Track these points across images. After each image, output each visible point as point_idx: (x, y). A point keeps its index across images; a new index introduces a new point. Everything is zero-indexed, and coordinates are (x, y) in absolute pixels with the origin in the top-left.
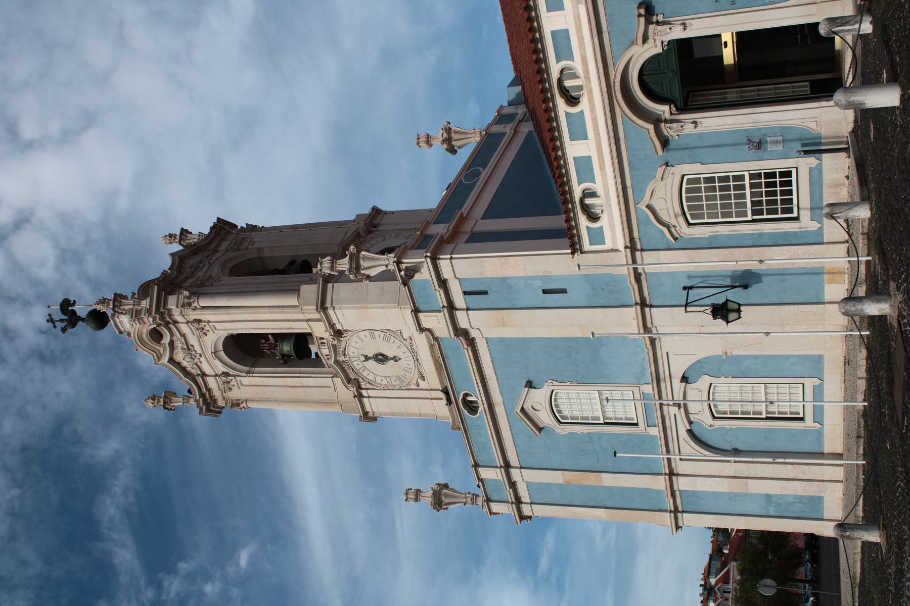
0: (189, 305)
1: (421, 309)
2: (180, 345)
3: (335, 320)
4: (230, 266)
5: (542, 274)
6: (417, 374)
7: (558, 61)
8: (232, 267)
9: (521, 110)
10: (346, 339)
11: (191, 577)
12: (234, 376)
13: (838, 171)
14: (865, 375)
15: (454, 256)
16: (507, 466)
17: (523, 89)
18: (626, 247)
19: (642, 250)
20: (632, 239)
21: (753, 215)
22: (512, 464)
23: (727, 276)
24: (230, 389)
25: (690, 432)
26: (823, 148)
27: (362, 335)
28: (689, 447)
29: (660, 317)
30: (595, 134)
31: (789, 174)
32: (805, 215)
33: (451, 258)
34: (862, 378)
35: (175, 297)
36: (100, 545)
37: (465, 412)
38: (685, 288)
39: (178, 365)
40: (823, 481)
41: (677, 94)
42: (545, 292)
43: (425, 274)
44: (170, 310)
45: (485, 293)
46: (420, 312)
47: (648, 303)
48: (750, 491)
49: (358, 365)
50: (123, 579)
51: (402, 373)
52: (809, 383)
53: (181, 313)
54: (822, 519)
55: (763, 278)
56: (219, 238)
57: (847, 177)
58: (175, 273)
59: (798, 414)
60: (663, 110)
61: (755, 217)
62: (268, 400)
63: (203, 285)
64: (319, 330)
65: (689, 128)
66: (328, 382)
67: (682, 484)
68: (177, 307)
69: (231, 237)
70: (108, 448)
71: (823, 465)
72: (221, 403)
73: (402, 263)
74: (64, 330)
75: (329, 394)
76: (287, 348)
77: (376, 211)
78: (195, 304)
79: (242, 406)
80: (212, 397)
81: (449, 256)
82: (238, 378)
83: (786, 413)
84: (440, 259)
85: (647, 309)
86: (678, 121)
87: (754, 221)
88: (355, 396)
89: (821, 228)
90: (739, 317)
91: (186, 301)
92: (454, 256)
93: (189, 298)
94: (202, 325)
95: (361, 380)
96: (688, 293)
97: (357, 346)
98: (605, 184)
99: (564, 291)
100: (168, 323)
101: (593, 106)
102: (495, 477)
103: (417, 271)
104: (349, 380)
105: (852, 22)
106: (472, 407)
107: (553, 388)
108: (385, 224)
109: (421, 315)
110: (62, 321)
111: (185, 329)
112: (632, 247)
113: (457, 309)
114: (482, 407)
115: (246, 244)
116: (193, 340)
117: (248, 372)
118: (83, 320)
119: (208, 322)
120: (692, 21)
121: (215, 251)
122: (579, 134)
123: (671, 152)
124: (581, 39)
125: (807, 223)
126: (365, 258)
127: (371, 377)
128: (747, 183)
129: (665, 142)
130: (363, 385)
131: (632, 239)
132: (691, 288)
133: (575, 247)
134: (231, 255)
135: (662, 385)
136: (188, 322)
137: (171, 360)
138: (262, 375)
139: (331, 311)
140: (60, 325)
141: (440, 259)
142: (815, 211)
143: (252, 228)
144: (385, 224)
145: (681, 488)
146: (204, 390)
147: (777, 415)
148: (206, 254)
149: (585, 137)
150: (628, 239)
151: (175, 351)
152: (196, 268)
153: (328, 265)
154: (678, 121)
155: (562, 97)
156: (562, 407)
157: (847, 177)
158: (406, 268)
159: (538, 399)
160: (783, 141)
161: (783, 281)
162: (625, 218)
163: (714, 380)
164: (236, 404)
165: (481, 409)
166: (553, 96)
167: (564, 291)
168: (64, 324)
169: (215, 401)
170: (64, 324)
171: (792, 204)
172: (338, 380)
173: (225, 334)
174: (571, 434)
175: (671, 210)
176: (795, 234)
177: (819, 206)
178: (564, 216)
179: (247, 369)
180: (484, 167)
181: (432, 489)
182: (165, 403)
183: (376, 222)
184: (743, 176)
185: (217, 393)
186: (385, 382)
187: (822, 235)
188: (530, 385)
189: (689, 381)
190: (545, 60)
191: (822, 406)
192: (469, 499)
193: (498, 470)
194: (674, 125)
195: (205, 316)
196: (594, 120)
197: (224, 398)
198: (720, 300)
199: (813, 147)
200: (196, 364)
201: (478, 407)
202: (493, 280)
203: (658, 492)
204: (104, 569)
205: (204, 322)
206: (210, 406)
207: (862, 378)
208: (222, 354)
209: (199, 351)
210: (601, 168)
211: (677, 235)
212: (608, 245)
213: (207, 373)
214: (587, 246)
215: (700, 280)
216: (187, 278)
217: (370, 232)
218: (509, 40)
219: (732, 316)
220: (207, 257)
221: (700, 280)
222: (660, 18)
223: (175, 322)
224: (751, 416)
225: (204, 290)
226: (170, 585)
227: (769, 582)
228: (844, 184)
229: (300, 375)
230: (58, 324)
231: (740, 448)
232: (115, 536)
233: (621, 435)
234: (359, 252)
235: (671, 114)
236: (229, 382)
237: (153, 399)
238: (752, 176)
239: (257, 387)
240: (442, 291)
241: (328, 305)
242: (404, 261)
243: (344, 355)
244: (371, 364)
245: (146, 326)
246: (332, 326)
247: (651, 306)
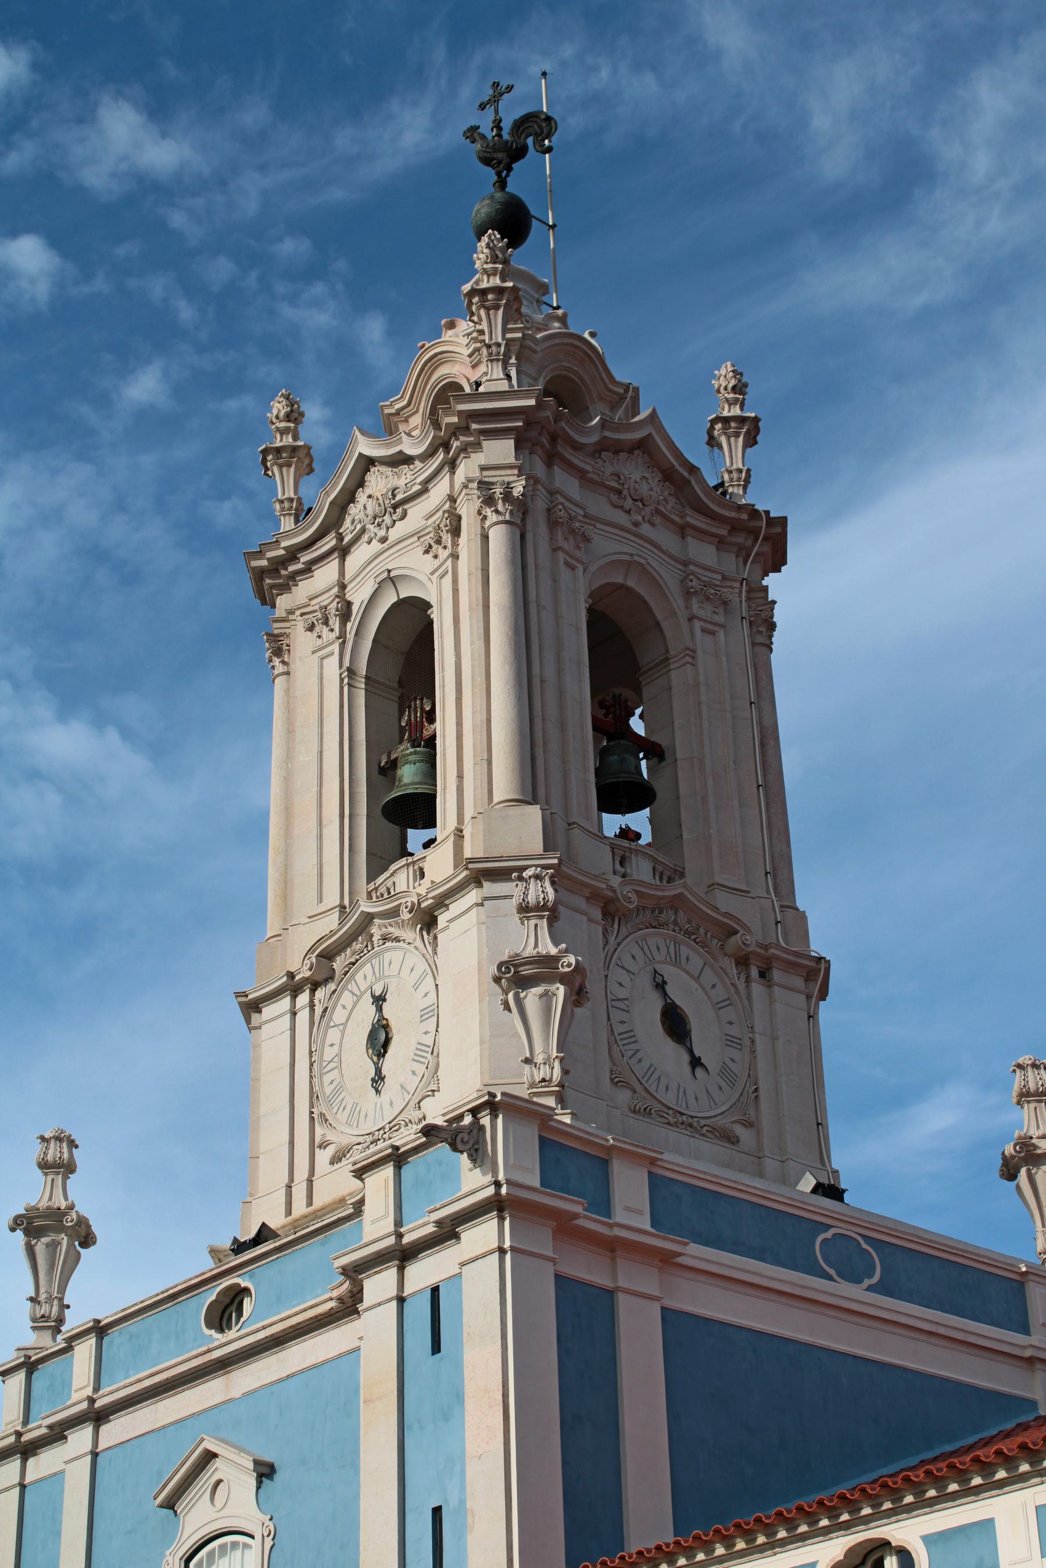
0: (489, 501)
1: (406, 1170)
2: (401, 482)
3: (456, 907)
4: (631, 583)
5: (469, 1505)
6: (346, 1141)
8: (629, 590)
10: (418, 943)
12: (342, 635)
15: (508, 1257)
16: (98, 1417)
24: (311, 628)
27: (428, 984)
33: (502, 1251)
35: (512, 460)
39: (358, 482)
42: (437, 1511)
44: (477, 446)
46: (398, 1168)
49: (364, 977)
51: (349, 1102)
53: (470, 480)
56: (724, 532)
62: (290, 731)
64: (441, 866)
66: (332, 898)
68: (483, 468)
69: (730, 563)
73: (494, 1117)
74: (472, 133)
76: (408, 774)
77: (815, 974)
78: (492, 518)
79: (276, 661)
80: (293, 577)
81: (507, 1244)
82: (336, 647)
84: (502, 1219)
88: (291, 975)
91: (498, 491)
93: (507, 496)
94: (447, 539)
95: (332, 986)
97: (406, 971)
100: (447, 446)
103: (473, 1159)
104: (328, 956)
106: (226, 1311)
109: (388, 1171)
110: (497, 125)
111: (440, 490)
113: (401, 1269)
114: (235, 1339)
115: (704, 611)
116: (417, 514)
117: (351, 672)
118: (502, 184)
119: (455, 556)
121: (683, 530)
126: (547, 997)
127: (339, 1016)
134: (669, 576)
136: (452, 499)
137: (367, 463)
138: (347, 710)
139: (473, 896)
141: (502, 1219)
143: (763, 622)
144: (772, 1000)
146: (306, 557)
148: (671, 506)
151: (387, 470)
153: (531, 899)
155: (850, 1552)
158: (482, 1128)
164: (279, 647)
165: (219, 1338)
166: (846, 1526)
168: (487, 129)
170: (487, 129)
172: (332, 921)
173: (432, 598)
178: (671, 1539)
179: (362, 668)
180: (881, 1288)
183: (777, 975)
185: (303, 589)
186: (329, 1053)
188: (265, 1472)
192: (44, 1309)
195: (467, 543)
197: (291, 612)
200: (363, 530)
201: (221, 1330)
202: (458, 1366)
205: (455, 544)
206: (272, 578)
208: (389, 599)
209: (394, 534)
213: (349, 559)
216: (582, 475)
217: (743, 961)
220: (658, 512)
223: (452, 465)
229: (347, 817)
230: (490, 113)
234: (563, 979)
236: (326, 623)
237: (288, 417)
239: (315, 695)
240: (431, 1229)
241: (490, 888)
243: (385, 938)
244: (367, 1014)
246: (442, 902)
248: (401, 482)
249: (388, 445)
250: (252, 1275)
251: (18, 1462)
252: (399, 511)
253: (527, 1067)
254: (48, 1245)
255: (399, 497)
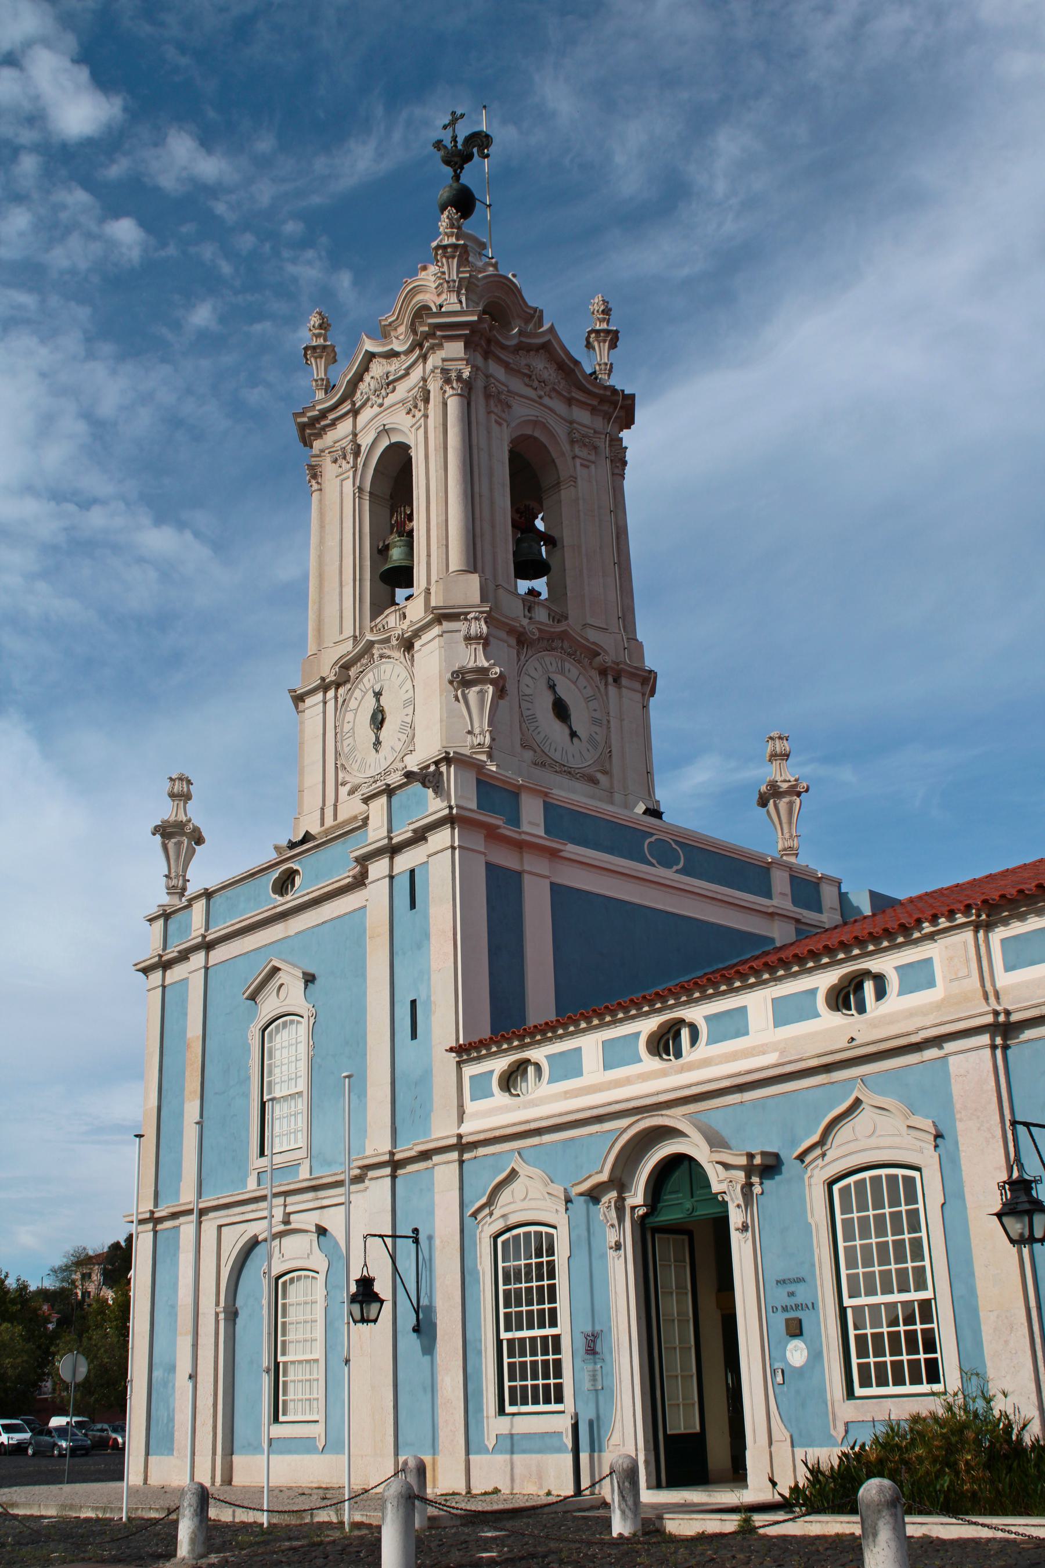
0: (448, 381)
1: (394, 799)
2: (392, 369)
4: (537, 434)
6: (357, 781)
7: (708, 1018)
8: (536, 439)
9: (829, 917)
10: (402, 659)
11: (325, 294)
12: (355, 466)
13: (549, 1478)
14: (237, 1520)
15: (457, 852)
16: (208, 946)
17: (865, 918)
18: (460, 1137)
19: (461, 1162)
20: (475, 1145)
21: (508, 1340)
22: (212, 953)
23: (431, 1301)
24: (335, 461)
25: (254, 1243)
26: (584, 1457)
28: (234, 1240)
29: (378, 1190)
30: (610, 1082)
31: (559, 1400)
32: (502, 1425)
33: (453, 848)
34: (234, 1516)
35: (462, 355)
36: (379, 111)
37: (275, 874)
38: (416, 1231)
39: (365, 368)
40: (193, 1454)
41: (666, 1217)
42: (413, 1003)
43: (435, 806)
44: (440, 346)
45: (413, 906)
46: (390, 797)
47: (400, 1172)
48: (178, 1338)
49: (369, 680)
50: (320, 164)
51: (359, 757)
52: (318, 1430)
54: (147, 1454)
55: (428, 1358)
56: (595, 403)
57: (549, 1494)
58: (514, 342)
59: (284, 1414)
60: (637, 1197)
61: (505, 1343)
62: (322, 526)
63: (488, 396)
64: (416, 611)
65: (612, 1237)
66: (348, 631)
67: (187, 1227)
68: (444, 360)
69: (599, 423)
70: (559, 96)
71: (214, 1453)
72: (317, 444)
73: (448, 766)
75: (331, 634)
76: (396, 554)
77: (647, 681)
78: (450, 392)
79: (313, 482)
80: (324, 428)
82: (351, 473)
83: (285, 1394)
84: (453, 829)
85: (388, 1171)
86: (621, 1219)
87: (843, 1311)
88: (323, 679)
89: (487, 1451)
90: (355, 1322)
91: (453, 375)
92: (457, 852)
93: (459, 378)
94: (421, 405)
95: (348, 686)
96: (408, 1238)
98: (544, 1099)
99: (414, 1035)
100: (421, 346)
101: (649, 1078)
102: (194, 927)
103: (436, 792)
104: (346, 667)
105: (623, 1506)
107: (306, 1017)
108: (620, 696)
110: (454, 139)
111: (417, 374)
112: (462, 1146)
113: (392, 859)
114: (290, 900)
116: (402, 389)
117: (361, 489)
118: (457, 177)
119: (426, 416)
120: (750, 1242)
121: (570, 401)
122: (615, 1056)
123: (584, 1207)
124: (734, 1056)
125: (495, 1426)
127: (353, 704)
128: (548, 1331)
129: (593, 1196)
130: (342, 691)
131: (475, 1145)
132: (416, 1241)
133: (465, 1052)
134: (561, 431)
135: (310, 1195)
137: (371, 356)
138: (357, 512)
139: (436, 630)
140: (446, 137)
141: (453, 829)
142: (508, 1441)
143: (619, 461)
144: (620, 696)
145: (182, 1228)
146: (332, 416)
147: (281, 1379)
148: (562, 386)
149: (607, 1067)
150: (471, 1139)
151: (384, 361)
152: (528, 377)
153: (473, 632)
154: (621, 1219)
156: (285, 1033)
157: (549, 1494)
158: (441, 773)
159: (291, 993)
160: (596, 1390)
161: (425, 1390)
162: (497, 1133)
163: (321, 1278)
164: (315, 473)
165: (280, 899)
166: (659, 1011)
167: (414, 1035)
169: (319, 435)
171: (522, 1404)
174: (247, 1049)
175: (512, 1207)
176: (480, 1410)
177: (516, 1448)
179: (367, 487)
181: (189, 821)
182: (314, 348)
183: (624, 681)
184: (926, 1289)
185: (330, 437)
186: (347, 727)
187: (479, 1452)
188: (309, 979)
189: (321, 1237)
190: (705, 998)
191: (262, 1452)
192: (174, 882)
193: (202, 931)
194: (613, 1214)
196: (627, 1081)
197: (322, 451)
198: (382, 1287)
199: (585, 1438)
200: (368, 399)
201: (282, 895)
202: (426, 917)
203: (177, 1193)
204: (336, 127)
205: (426, 409)
206: (311, 429)
207: (234, 1516)
208: (384, 443)
209: (387, 402)
210: (566, 1092)
211: (808, 1159)
212: (470, 1106)
214: (470, 1070)
215: (427, 1257)
216: (506, 366)
217: (603, 672)
218: (957, 885)
219: (356, 1308)
220: (554, 390)
221: (427, 1257)
222: (757, 1189)
223: (424, 358)
224: (280, 1339)
225: (479, 399)
226: (310, 263)
227: (83, 1370)
228: (541, 1488)
229: (358, 580)
230: (450, 130)
231: (238, 1320)
232: (397, 136)
233: (248, 1130)
235: (633, 1208)
236: (345, 458)
237: (321, 326)
238: (557, 1338)
239: (337, 509)
240: (410, 834)
241: (447, 625)
242: (452, 769)
243: (381, 656)
244: (370, 703)
245: (435, 298)
246: (417, 634)
247: (394, 1177)
248: (392, 369)
249: (384, 345)
250: (300, 862)
251: (161, 972)
252: (391, 387)
253: (469, 736)
254: (175, 844)
255: (391, 378)
